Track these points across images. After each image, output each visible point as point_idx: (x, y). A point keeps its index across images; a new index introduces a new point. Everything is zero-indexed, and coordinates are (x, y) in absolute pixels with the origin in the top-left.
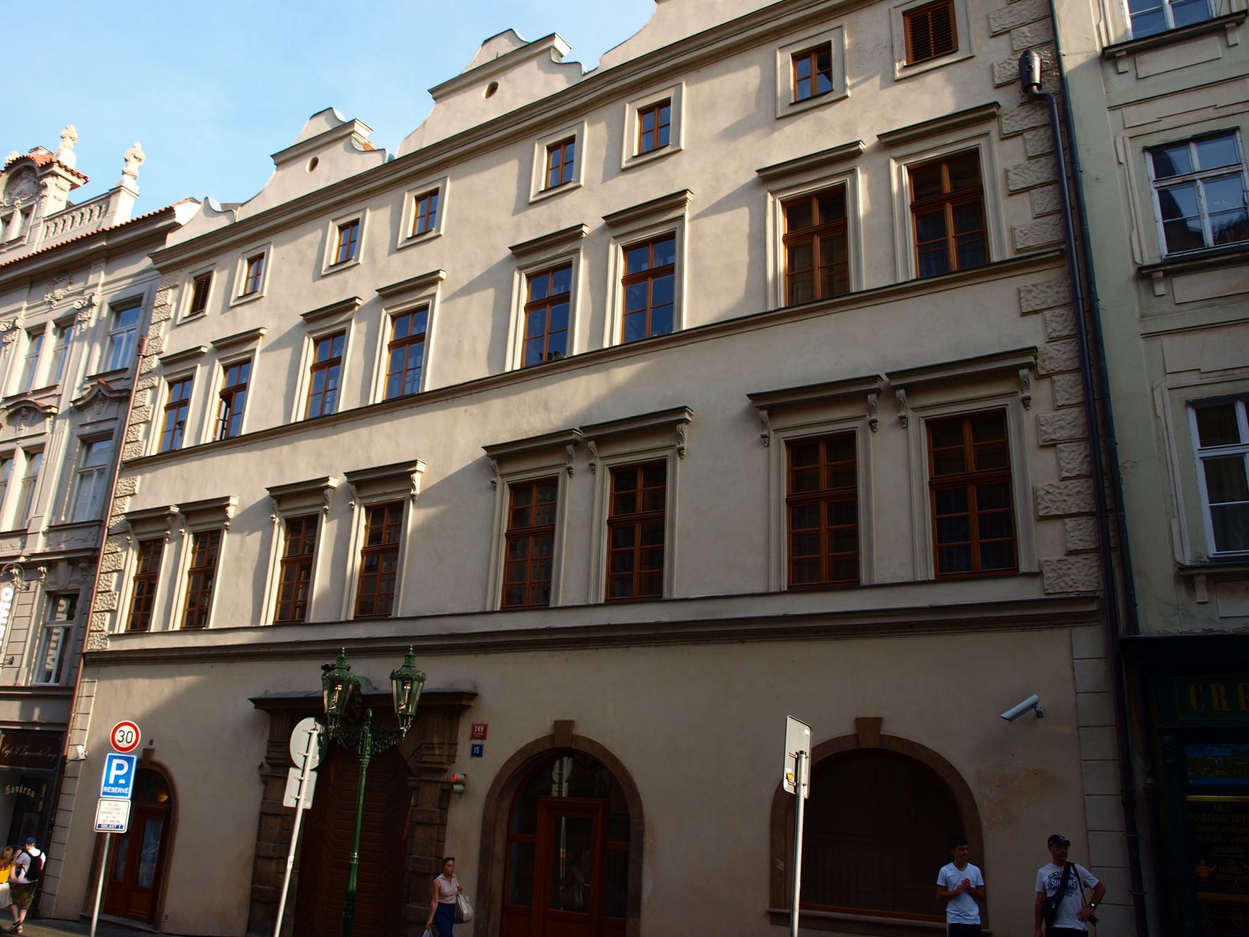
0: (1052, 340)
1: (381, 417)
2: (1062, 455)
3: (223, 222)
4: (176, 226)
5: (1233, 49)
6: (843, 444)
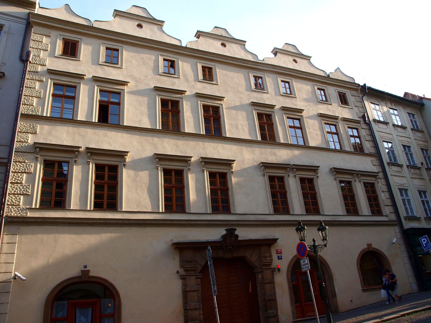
1: (208, 140)
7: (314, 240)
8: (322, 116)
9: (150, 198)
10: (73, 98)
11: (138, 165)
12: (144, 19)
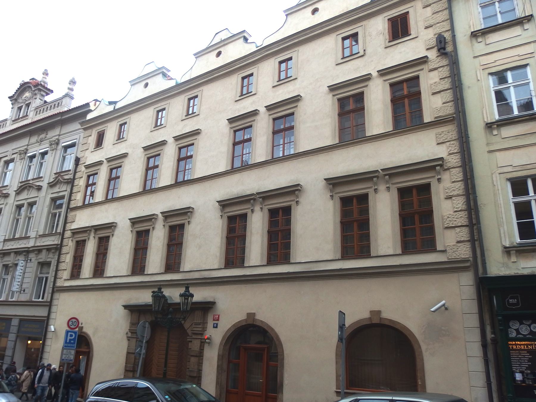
0: (450, 154)
2: (454, 202)
3: (111, 108)
4: (91, 111)
5: (526, 31)
6: (363, 199)
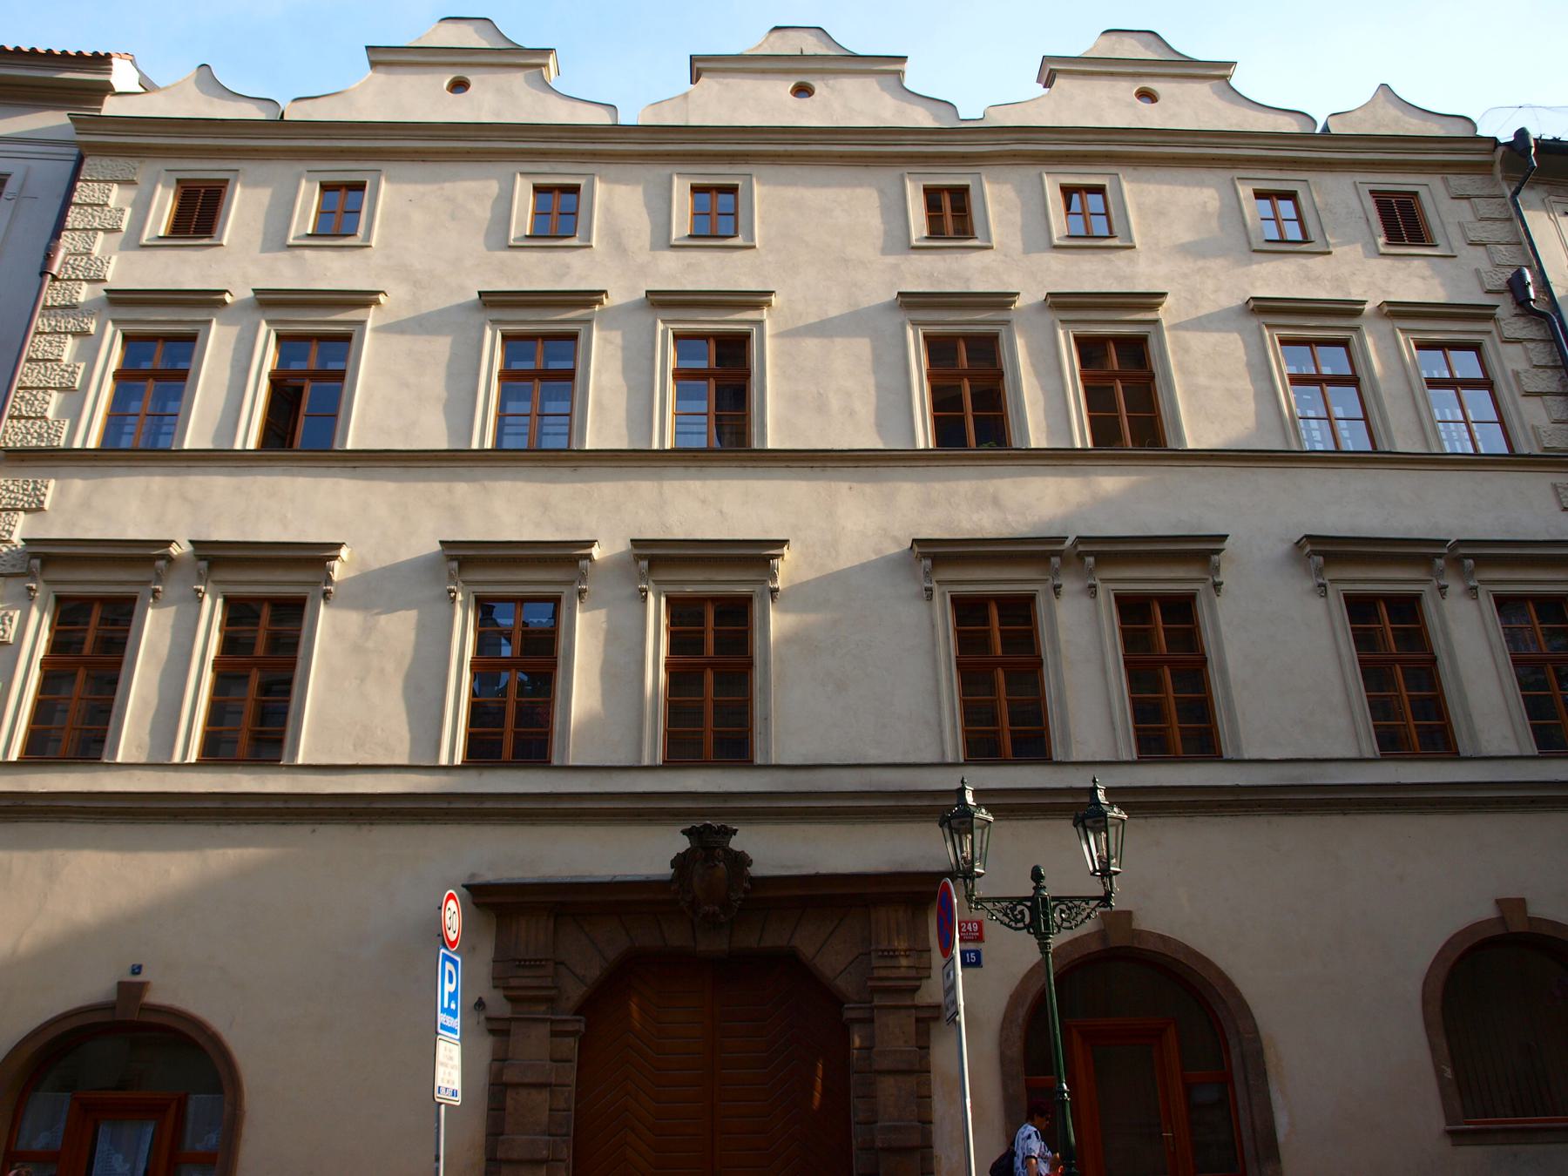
7: (1037, 875)
8: (1262, 308)
9: (410, 711)
10: (569, 375)
11: (377, 590)
12: (1156, 65)
